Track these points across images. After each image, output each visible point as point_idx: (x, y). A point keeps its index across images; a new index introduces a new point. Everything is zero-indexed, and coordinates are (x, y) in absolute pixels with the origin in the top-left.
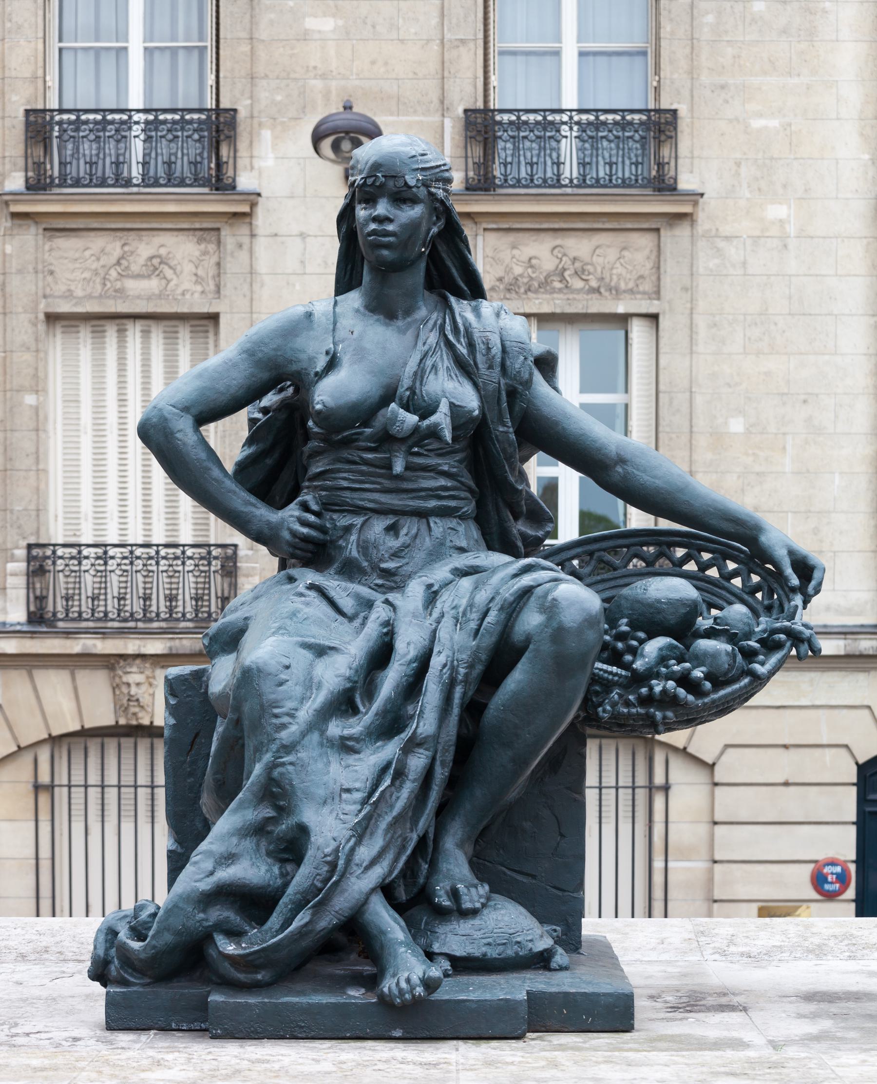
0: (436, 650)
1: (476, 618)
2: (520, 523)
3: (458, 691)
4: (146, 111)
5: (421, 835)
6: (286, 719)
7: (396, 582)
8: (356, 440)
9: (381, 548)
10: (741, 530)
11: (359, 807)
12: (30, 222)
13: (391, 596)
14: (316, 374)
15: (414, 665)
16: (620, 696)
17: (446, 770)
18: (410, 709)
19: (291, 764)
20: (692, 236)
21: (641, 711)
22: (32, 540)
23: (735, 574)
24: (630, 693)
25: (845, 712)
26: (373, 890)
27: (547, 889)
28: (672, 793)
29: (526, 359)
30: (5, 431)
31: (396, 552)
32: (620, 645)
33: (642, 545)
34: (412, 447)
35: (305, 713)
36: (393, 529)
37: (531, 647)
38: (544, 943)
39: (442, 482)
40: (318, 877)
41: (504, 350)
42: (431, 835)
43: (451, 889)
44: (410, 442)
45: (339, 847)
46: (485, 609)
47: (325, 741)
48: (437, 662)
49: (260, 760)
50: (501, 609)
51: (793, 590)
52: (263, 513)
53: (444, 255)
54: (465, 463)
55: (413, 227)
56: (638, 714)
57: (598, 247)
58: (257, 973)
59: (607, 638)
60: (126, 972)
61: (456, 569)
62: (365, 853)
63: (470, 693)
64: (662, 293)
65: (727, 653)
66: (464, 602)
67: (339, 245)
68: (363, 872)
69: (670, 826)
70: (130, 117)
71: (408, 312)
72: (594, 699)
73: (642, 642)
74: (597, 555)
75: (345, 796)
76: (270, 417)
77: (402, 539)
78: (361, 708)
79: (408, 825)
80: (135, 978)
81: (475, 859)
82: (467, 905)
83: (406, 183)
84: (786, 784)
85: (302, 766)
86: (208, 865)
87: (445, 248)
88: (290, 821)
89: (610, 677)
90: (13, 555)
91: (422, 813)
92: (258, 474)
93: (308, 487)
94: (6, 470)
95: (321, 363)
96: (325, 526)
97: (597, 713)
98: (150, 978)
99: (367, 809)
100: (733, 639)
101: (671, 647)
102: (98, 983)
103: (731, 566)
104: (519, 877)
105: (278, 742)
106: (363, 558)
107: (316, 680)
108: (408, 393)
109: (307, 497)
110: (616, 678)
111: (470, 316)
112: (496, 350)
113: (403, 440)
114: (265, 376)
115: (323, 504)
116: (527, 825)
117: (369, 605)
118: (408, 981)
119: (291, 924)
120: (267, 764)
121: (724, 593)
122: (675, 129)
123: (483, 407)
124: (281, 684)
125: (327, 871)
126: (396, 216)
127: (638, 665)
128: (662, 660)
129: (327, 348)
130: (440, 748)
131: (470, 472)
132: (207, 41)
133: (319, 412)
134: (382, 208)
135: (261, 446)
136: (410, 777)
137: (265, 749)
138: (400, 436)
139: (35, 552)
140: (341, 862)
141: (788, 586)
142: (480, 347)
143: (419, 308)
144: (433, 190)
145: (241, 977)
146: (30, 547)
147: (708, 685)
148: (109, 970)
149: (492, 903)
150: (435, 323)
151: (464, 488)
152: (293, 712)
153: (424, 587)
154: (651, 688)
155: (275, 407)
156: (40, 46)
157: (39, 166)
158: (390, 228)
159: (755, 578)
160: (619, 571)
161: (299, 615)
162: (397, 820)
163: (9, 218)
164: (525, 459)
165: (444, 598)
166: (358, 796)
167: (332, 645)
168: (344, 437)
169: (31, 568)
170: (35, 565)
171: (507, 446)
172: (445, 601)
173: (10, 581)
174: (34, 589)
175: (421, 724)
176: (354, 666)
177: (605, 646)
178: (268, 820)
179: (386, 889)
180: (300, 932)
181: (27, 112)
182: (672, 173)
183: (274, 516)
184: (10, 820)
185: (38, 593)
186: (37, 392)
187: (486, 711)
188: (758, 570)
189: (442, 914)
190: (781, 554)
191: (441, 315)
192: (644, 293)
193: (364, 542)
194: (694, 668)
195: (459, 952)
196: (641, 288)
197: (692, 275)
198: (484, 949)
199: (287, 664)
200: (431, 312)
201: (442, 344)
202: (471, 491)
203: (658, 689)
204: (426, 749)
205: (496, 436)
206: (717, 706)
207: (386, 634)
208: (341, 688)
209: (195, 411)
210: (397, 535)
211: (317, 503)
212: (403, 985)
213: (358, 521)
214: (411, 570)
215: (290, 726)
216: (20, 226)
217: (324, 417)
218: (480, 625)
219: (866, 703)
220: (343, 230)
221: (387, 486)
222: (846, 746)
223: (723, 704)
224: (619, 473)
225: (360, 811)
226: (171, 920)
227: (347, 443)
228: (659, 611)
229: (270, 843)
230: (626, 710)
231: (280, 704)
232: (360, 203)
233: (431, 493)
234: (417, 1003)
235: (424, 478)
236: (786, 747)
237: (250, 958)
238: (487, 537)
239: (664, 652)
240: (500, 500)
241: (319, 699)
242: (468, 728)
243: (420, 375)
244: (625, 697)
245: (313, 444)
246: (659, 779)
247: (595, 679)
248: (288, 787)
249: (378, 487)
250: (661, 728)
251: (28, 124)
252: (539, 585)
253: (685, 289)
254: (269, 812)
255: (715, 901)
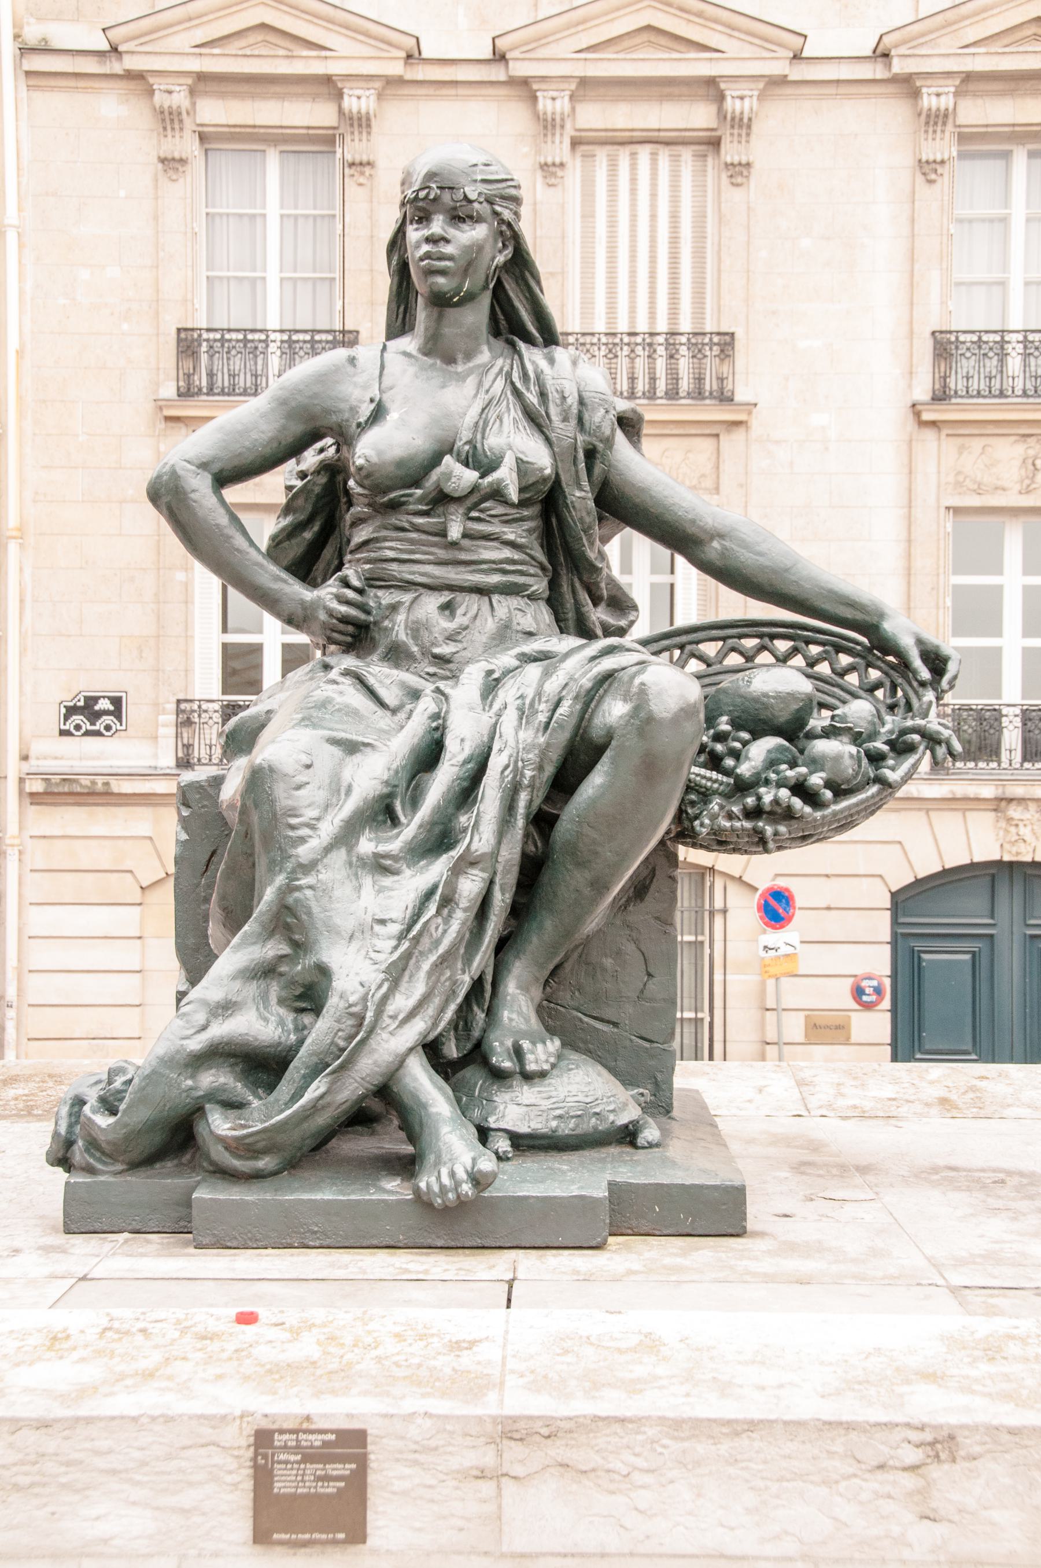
0: (495, 748)
1: (546, 710)
2: (600, 609)
3: (523, 797)
4: (282, 331)
5: (476, 978)
6: (304, 832)
7: (451, 671)
8: (404, 503)
9: (434, 629)
10: (859, 616)
11: (394, 943)
12: (181, 425)
13: (442, 685)
14: (359, 425)
15: (469, 766)
16: (722, 807)
17: (507, 895)
18: (463, 819)
19: (311, 887)
20: (747, 440)
21: (748, 825)
22: (181, 697)
23: (851, 668)
24: (734, 803)
25: (879, 846)
26: (411, 1050)
27: (631, 1040)
28: (728, 915)
29: (607, 412)
30: (159, 602)
31: (452, 635)
32: (719, 747)
33: (740, 637)
34: (470, 509)
35: (329, 828)
36: (448, 608)
37: (613, 743)
38: (630, 1114)
39: (507, 553)
40: (340, 1034)
41: (581, 402)
42: (489, 978)
43: (513, 1046)
44: (469, 502)
45: (367, 994)
46: (557, 698)
47: (354, 859)
48: (497, 763)
49: (272, 881)
50: (576, 698)
51: (923, 684)
52: (297, 590)
53: (511, 294)
54: (535, 535)
55: (474, 251)
56: (743, 829)
57: (666, 450)
58: (256, 1158)
59: (705, 739)
60: (92, 1155)
61: (523, 654)
62: (402, 1002)
63: (537, 802)
64: (722, 488)
65: (851, 756)
66: (530, 693)
67: (389, 281)
68: (398, 1027)
69: (728, 943)
70: (267, 336)
71: (469, 356)
72: (690, 811)
73: (745, 743)
74: (688, 648)
75: (377, 928)
76: (309, 481)
77: (460, 620)
78: (403, 819)
79: (459, 965)
80: (105, 1163)
81: (545, 1002)
82: (531, 1067)
83: (465, 196)
84: (829, 908)
85: (324, 890)
86: (201, 1018)
87: (513, 285)
88: (310, 960)
89: (709, 784)
90: (164, 709)
91: (477, 950)
92: (296, 548)
93: (350, 562)
94: (158, 636)
95: (366, 410)
96: (367, 604)
97: (693, 827)
98: (123, 1162)
99: (405, 945)
100: (857, 738)
101: (780, 749)
102: (61, 1169)
103: (845, 660)
104: (598, 1025)
105: (293, 860)
106: (411, 641)
107: (345, 784)
108: (467, 447)
109: (349, 572)
110: (716, 786)
111: (543, 364)
112: (572, 400)
113: (459, 500)
114: (297, 429)
115: (367, 579)
116: (608, 962)
117: (415, 695)
118: (452, 1174)
119: (302, 1096)
120: (280, 889)
121: (836, 690)
122: (733, 348)
123: (557, 467)
124: (299, 787)
125: (353, 1026)
126: (454, 237)
127: (745, 769)
128: (771, 763)
129: (372, 395)
130: (500, 868)
131: (542, 547)
132: (335, 272)
133: (360, 469)
134: (438, 225)
135: (302, 517)
136: (461, 906)
137: (277, 868)
138: (456, 495)
139: (183, 706)
140: (370, 1015)
141: (917, 680)
142: (553, 396)
143: (481, 352)
144: (498, 209)
145: (237, 1164)
146: (179, 702)
147: (828, 794)
148: (73, 1152)
149: (563, 1064)
150: (501, 370)
151: (534, 563)
152: (314, 822)
153: (484, 674)
154: (759, 798)
155: (313, 469)
156: (190, 273)
157: (188, 376)
158: (448, 249)
159: (874, 674)
160: (714, 667)
161: (329, 707)
162: (444, 960)
163: (163, 422)
164: (605, 540)
165: (508, 686)
166: (395, 929)
167: (366, 741)
168: (391, 500)
169: (180, 720)
170: (183, 717)
171: (584, 514)
172: (507, 693)
173: (162, 731)
174: (182, 738)
175: (476, 838)
176: (394, 766)
177: (703, 748)
178: (282, 957)
179: (431, 1049)
180: (314, 1106)
181: (179, 330)
182: (730, 387)
183: (308, 595)
184: (158, 937)
185: (185, 741)
186: (186, 570)
187: (558, 824)
188: (879, 663)
189: (499, 1076)
190: (907, 643)
191: (509, 361)
192: (706, 489)
193: (414, 622)
194: (811, 773)
195: (523, 1129)
196: (703, 485)
197: (747, 473)
198: (554, 1124)
199: (309, 763)
200: (495, 358)
201: (509, 393)
202: (543, 568)
203: (767, 799)
204: (483, 870)
205: (572, 502)
206: (839, 820)
207: (436, 729)
208: (377, 793)
209: (216, 467)
210: (453, 615)
211: (359, 579)
212: (446, 1180)
213: (407, 597)
214: (469, 655)
215: (310, 840)
216: (173, 428)
217: (366, 475)
218: (551, 718)
219: (897, 839)
220: (394, 262)
221: (442, 556)
222: (880, 876)
223: (846, 817)
224: (716, 549)
225: (396, 948)
226: (149, 1089)
227: (395, 506)
228: (766, 707)
229: (283, 988)
230: (728, 824)
231: (298, 813)
232: (411, 223)
233: (494, 566)
234: (462, 1205)
235: (486, 548)
236: (827, 876)
237: (247, 1141)
238: (562, 625)
239: (773, 756)
240: (576, 580)
241: (349, 807)
242: (536, 846)
243: (481, 426)
244: (727, 808)
245: (356, 510)
246: (718, 904)
247: (690, 787)
248: (304, 917)
249: (431, 557)
250: (771, 845)
251: (179, 340)
252: (623, 669)
253: (741, 486)
254: (285, 949)
255: (768, 1010)
